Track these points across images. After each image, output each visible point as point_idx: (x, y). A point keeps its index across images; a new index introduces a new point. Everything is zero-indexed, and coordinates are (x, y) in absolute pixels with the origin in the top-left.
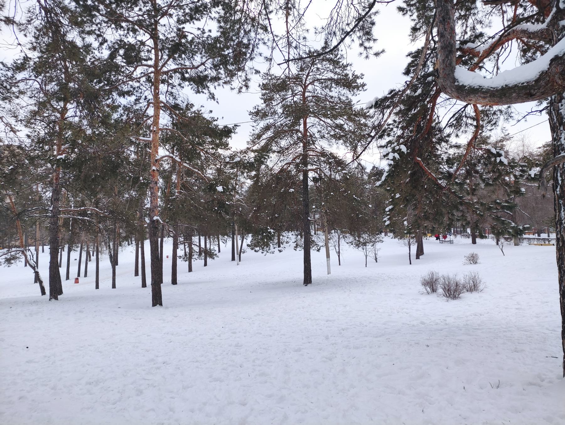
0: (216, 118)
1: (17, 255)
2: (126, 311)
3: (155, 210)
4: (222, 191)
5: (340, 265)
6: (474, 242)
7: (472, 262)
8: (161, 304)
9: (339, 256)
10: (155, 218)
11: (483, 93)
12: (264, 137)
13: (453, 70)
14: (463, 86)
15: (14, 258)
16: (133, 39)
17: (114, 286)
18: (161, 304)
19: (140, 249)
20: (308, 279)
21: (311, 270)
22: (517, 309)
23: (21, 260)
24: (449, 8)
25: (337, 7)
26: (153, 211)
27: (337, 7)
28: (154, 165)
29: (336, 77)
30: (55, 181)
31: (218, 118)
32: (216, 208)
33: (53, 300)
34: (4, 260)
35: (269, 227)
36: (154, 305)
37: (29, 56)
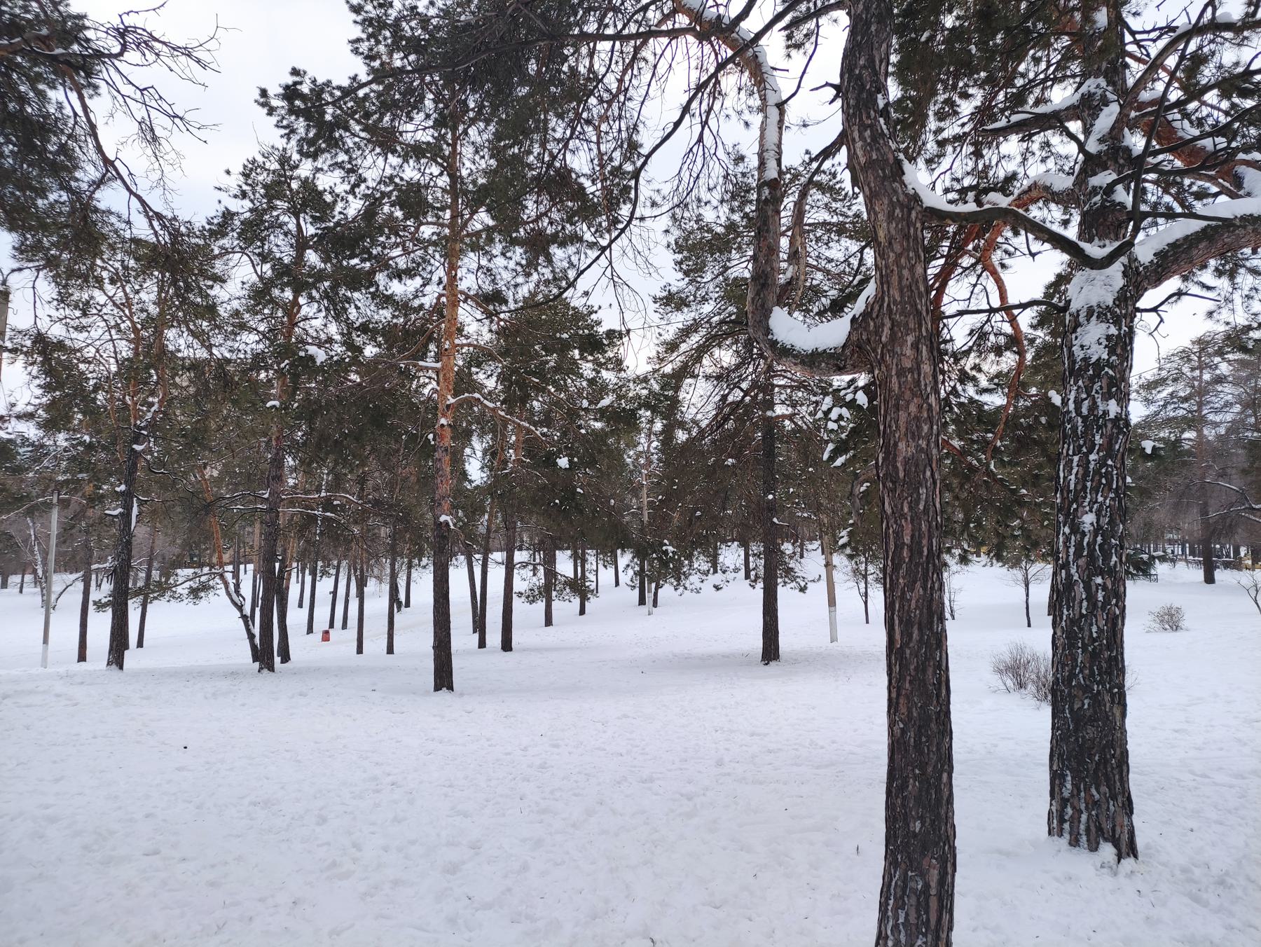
0: (595, 309)
1: (211, 583)
2: (384, 698)
3: (443, 502)
4: (568, 466)
5: (867, 622)
6: (1209, 579)
7: (1167, 626)
8: (451, 688)
9: (866, 603)
10: (443, 518)
11: (795, 357)
12: (684, 347)
13: (767, 314)
14: (776, 342)
15: (205, 587)
16: (416, 172)
17: (390, 650)
18: (451, 688)
19: (579, 569)
20: (771, 651)
21: (777, 632)
22: (1176, 731)
23: (217, 592)
24: (770, 213)
25: (689, 161)
26: (440, 504)
27: (689, 161)
28: (444, 415)
29: (835, 220)
30: (274, 443)
31: (600, 307)
32: (557, 501)
33: (265, 671)
34: (186, 591)
35: (666, 541)
36: (437, 688)
37: (233, 209)
